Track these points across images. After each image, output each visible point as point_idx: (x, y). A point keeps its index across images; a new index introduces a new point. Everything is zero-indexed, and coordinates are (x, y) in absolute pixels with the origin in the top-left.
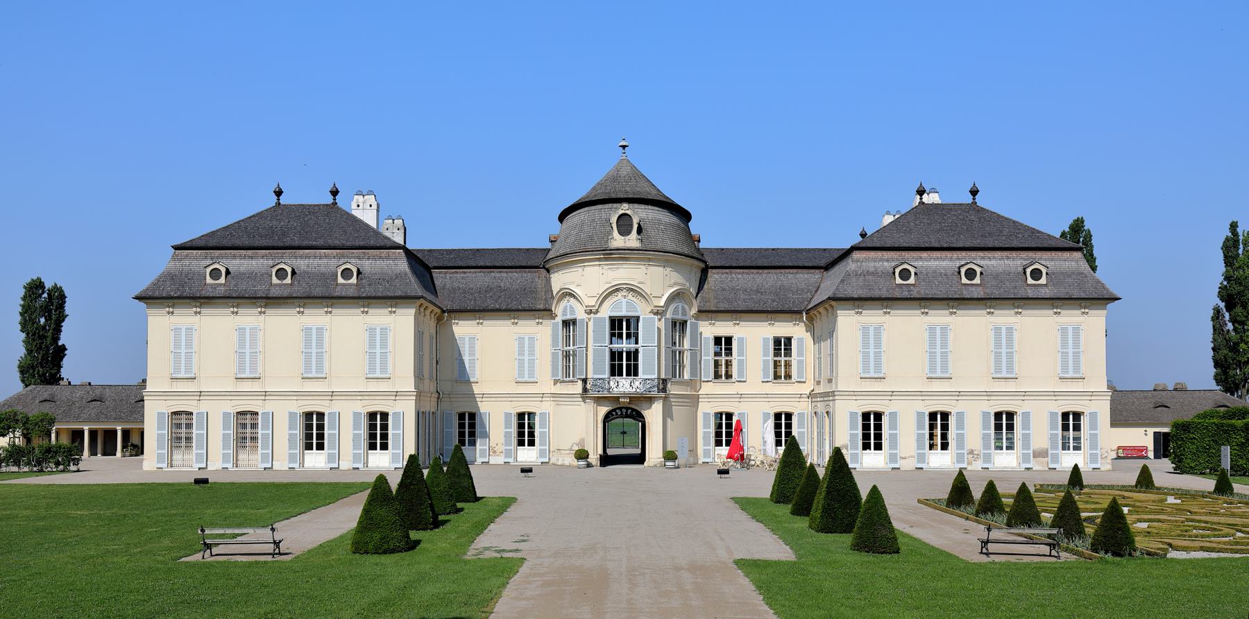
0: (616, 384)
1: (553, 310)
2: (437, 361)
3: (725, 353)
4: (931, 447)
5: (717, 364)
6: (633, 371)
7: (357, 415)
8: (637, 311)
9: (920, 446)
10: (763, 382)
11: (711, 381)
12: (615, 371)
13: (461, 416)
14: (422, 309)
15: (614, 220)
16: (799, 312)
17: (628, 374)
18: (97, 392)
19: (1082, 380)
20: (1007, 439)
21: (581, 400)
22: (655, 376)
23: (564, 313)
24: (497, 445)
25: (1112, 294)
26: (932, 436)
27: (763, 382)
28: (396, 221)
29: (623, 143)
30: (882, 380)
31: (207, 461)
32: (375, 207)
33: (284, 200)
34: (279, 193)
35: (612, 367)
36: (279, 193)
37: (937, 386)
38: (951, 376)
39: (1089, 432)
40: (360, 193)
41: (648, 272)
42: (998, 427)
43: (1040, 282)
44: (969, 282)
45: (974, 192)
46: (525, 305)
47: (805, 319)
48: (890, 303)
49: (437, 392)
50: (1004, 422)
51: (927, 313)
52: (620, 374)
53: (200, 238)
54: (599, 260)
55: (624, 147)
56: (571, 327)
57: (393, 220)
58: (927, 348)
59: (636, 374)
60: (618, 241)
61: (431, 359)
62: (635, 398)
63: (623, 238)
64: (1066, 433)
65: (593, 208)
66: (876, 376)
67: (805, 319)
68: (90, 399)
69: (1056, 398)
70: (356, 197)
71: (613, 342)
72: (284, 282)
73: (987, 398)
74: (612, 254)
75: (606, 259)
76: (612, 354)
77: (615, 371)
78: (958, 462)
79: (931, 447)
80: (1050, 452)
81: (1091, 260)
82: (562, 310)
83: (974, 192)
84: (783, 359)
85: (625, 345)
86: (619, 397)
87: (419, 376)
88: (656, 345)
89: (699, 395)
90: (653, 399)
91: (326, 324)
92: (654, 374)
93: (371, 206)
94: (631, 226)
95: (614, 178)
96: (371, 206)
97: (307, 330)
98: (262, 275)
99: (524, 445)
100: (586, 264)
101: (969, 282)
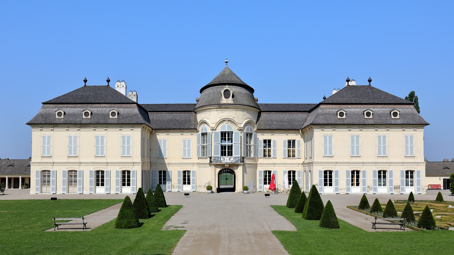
0: (224, 159)
1: (198, 129)
2: (150, 150)
3: (268, 146)
5: (265, 151)
6: (230, 154)
7: (117, 172)
8: (232, 129)
12: (223, 154)
13: (160, 172)
14: (144, 129)
15: (222, 92)
16: (298, 130)
17: (228, 155)
18: (11, 162)
20: (383, 181)
21: (209, 165)
22: (239, 156)
23: (202, 130)
24: (175, 184)
26: (352, 180)
28: (133, 93)
29: (226, 61)
30: (332, 157)
32: (125, 87)
33: (88, 84)
34: (85, 81)
35: (222, 152)
36: (85, 81)
37: (354, 160)
40: (119, 81)
41: (237, 113)
42: (380, 177)
45: (370, 81)
46: (186, 127)
47: (300, 133)
49: (150, 162)
50: (162, 174)
52: (225, 155)
54: (216, 108)
55: (227, 62)
56: (205, 136)
57: (132, 92)
59: (232, 155)
60: (224, 101)
61: (148, 149)
62: (231, 165)
63: (226, 99)
64: (407, 179)
66: (48, 156)
67: (300, 133)
68: (8, 165)
70: (117, 83)
71: (222, 142)
72: (88, 117)
73: (375, 165)
74: (222, 106)
75: (219, 108)
76: (222, 147)
77: (223, 154)
78: (336, 191)
79: (352, 185)
80: (401, 187)
81: (417, 108)
82: (201, 129)
84: (267, 149)
85: (227, 143)
86: (224, 164)
87: (143, 156)
88: (240, 143)
90: (238, 165)
91: (105, 135)
92: (239, 155)
93: (123, 86)
94: (230, 94)
95: (223, 75)
96: (123, 86)
98: (79, 115)
99: (408, 186)
100: (211, 110)
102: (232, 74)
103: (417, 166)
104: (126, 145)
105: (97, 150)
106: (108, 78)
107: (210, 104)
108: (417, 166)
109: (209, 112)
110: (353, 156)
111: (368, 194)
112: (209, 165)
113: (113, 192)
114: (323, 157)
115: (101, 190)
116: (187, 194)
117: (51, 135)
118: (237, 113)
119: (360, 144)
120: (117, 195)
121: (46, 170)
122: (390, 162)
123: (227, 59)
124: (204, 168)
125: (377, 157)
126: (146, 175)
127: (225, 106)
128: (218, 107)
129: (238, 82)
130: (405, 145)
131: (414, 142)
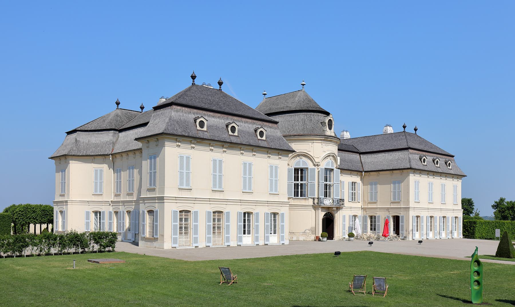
0: (333, 201)
4: (244, 233)
9: (175, 234)
10: (279, 194)
11: (351, 202)
19: (222, 192)
21: (312, 208)
25: (292, 149)
27: (279, 194)
29: (303, 83)
31: (135, 238)
33: (197, 81)
34: (193, 77)
36: (193, 77)
37: (217, 196)
38: (223, 190)
39: (194, 224)
41: (313, 146)
43: (263, 139)
44: (232, 134)
48: (281, 152)
51: (179, 146)
53: (172, 98)
54: (321, 140)
55: (303, 85)
56: (328, 172)
58: (269, 178)
65: (309, 113)
66: (187, 188)
69: (177, 201)
74: (328, 138)
75: (324, 140)
79: (181, 233)
83: (404, 127)
89: (164, 197)
90: (339, 209)
91: (191, 155)
97: (215, 161)
100: (314, 141)
101: (232, 134)
102: (311, 101)
103: (194, 203)
104: (185, 171)
105: (181, 178)
106: (220, 79)
107: (315, 134)
108: (194, 203)
109: (310, 144)
110: (182, 187)
111: (260, 246)
112: (312, 207)
113: (202, 245)
114: (415, 202)
115: (247, 240)
116: (420, 242)
117: (191, 155)
118: (313, 146)
119: (191, 170)
120: (266, 246)
121: (183, 210)
122: (257, 200)
123: (303, 81)
124: (297, 211)
125: (242, 192)
126: (279, 219)
127: (331, 138)
128: (324, 139)
129: (318, 109)
130: (243, 176)
131: (278, 176)
